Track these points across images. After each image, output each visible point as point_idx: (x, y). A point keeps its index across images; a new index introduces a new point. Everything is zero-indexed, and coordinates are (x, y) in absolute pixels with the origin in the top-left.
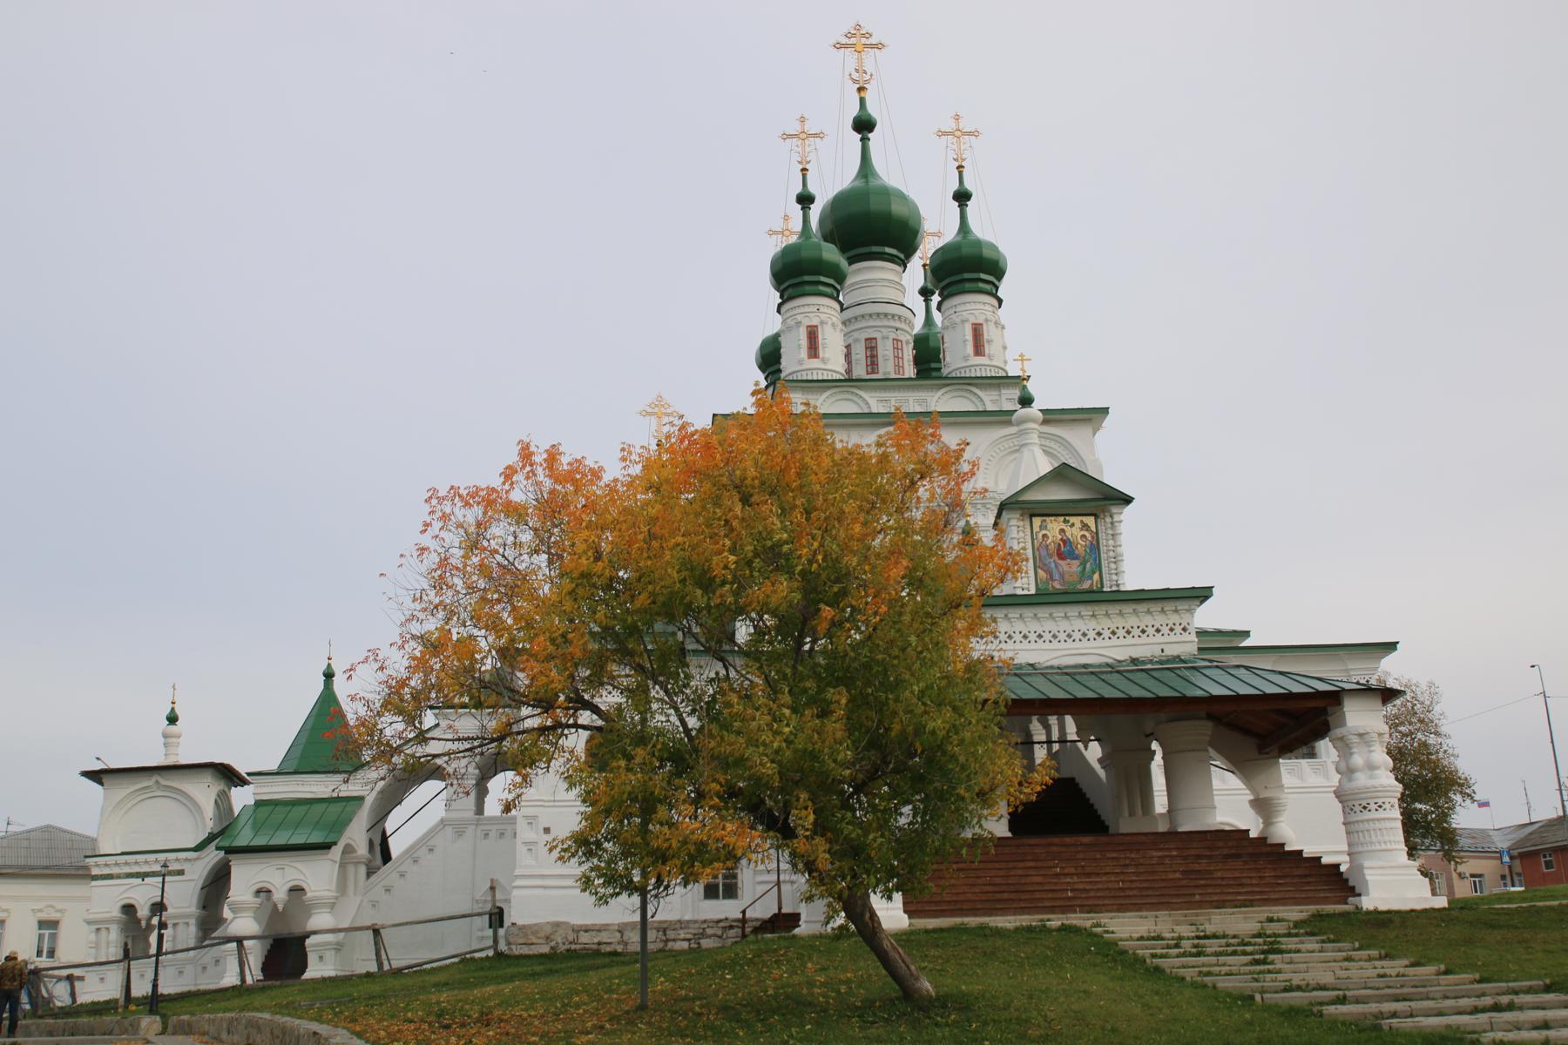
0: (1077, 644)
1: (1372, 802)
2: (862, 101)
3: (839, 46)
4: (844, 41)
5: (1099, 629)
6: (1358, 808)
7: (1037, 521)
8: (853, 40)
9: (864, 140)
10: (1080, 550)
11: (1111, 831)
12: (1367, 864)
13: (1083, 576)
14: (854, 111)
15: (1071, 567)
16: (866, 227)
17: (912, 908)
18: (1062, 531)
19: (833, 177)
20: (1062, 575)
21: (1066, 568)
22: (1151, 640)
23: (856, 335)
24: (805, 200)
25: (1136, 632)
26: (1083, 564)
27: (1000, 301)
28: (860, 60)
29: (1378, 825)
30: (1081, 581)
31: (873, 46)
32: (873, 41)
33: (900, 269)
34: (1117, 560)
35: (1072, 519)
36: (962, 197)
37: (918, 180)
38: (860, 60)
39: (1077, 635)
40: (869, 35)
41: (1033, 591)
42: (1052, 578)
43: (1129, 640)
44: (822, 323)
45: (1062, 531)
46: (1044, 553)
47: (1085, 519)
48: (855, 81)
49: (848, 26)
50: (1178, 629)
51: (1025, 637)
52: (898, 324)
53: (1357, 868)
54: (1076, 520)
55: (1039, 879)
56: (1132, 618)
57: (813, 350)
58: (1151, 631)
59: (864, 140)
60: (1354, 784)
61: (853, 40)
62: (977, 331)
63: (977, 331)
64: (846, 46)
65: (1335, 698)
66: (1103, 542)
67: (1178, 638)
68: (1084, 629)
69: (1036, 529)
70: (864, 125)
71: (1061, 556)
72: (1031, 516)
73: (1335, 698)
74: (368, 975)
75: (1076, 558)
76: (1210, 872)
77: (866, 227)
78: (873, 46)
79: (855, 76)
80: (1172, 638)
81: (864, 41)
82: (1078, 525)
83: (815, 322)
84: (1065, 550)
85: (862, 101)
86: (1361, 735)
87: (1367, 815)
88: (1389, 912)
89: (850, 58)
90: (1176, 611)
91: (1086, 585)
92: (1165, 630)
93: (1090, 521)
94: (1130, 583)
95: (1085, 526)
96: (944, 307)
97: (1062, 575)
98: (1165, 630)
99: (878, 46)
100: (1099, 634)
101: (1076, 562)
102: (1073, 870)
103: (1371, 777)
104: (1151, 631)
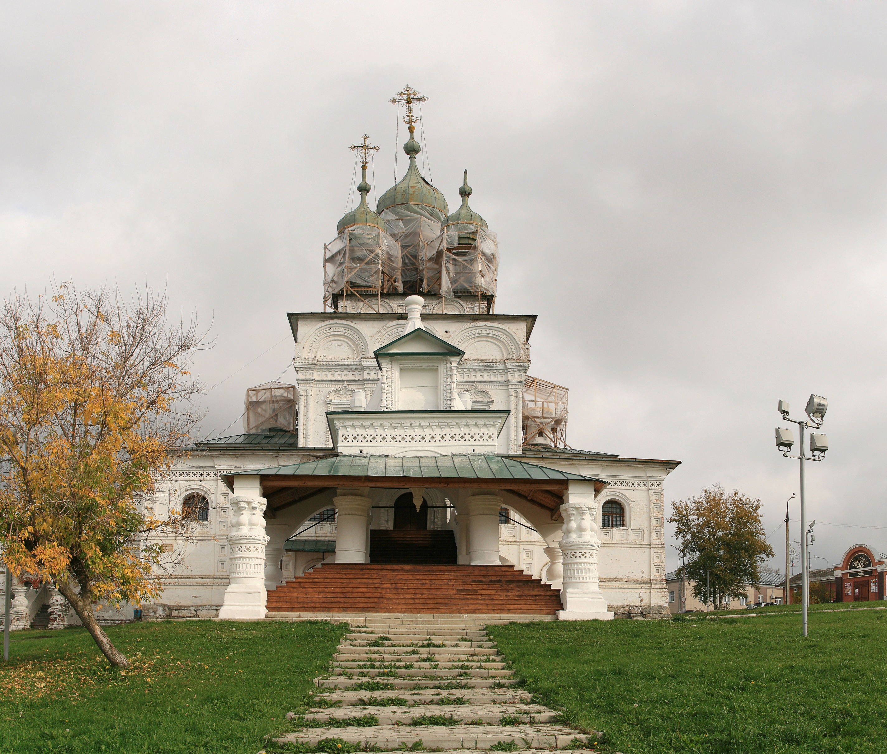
0: (418, 444)
1: (578, 552)
6: (578, 555)
11: (461, 560)
17: (273, 605)
19: (386, 176)
22: (467, 443)
24: (364, 189)
25: (457, 437)
39: (418, 438)
40: (415, 93)
43: (453, 442)
51: (627, 484)
53: (565, 592)
55: (365, 590)
58: (467, 437)
60: (568, 540)
65: (565, 483)
67: (485, 443)
73: (565, 483)
76: (476, 591)
78: (418, 100)
86: (577, 508)
87: (583, 560)
88: (576, 621)
92: (477, 437)
98: (477, 437)
99: (422, 99)
102: (389, 586)
103: (238, 531)
104: (467, 437)
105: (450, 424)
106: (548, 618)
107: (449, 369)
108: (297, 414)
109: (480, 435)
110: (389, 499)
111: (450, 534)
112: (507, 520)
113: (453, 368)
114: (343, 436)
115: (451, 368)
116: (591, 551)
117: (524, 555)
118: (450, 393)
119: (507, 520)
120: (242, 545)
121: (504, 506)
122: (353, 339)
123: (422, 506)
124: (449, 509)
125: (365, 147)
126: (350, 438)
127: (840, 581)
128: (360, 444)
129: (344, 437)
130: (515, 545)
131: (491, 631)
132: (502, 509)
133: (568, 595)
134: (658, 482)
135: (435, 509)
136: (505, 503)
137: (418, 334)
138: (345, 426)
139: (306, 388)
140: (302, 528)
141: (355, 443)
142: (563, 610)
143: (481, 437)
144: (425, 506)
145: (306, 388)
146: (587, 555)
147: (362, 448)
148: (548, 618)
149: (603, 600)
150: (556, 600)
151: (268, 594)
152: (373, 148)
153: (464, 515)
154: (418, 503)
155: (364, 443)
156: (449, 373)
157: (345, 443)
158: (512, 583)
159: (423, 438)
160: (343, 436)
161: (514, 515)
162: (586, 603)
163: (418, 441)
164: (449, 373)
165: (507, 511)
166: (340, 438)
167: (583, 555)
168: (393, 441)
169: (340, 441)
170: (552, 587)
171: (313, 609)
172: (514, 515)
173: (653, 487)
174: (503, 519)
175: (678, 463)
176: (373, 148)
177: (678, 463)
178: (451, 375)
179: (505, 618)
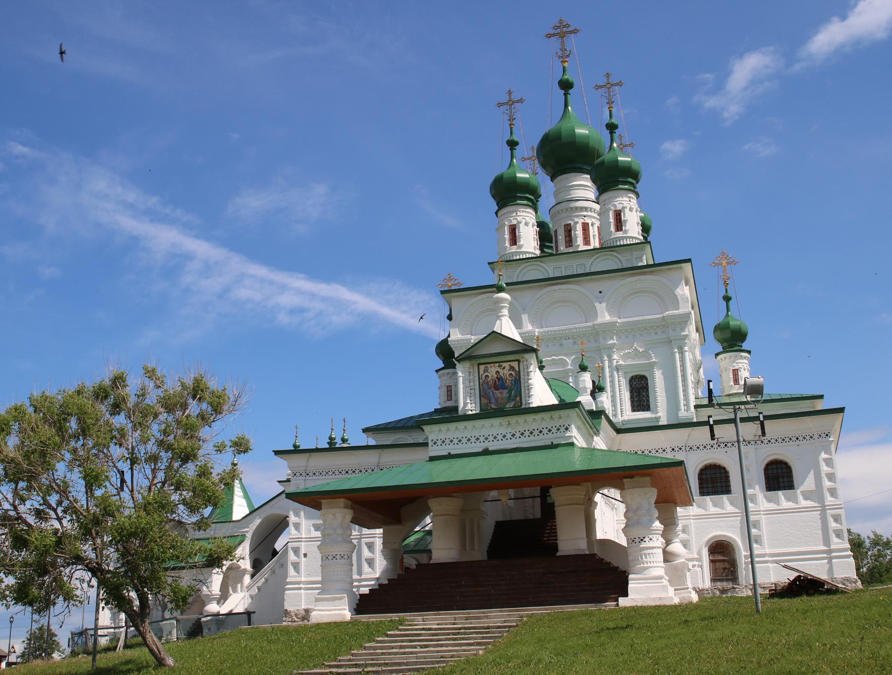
3: (549, 36)
4: (552, 32)
7: (482, 367)
13: (509, 399)
15: (502, 394)
18: (498, 372)
20: (497, 400)
21: (499, 395)
26: (510, 392)
28: (563, 43)
32: (570, 29)
34: (529, 388)
35: (504, 365)
38: (563, 43)
42: (490, 403)
44: (624, 208)
45: (498, 372)
46: (486, 387)
52: (585, 213)
57: (514, 240)
66: (522, 377)
69: (481, 372)
71: (496, 388)
72: (479, 365)
75: (506, 388)
81: (565, 29)
82: (508, 368)
89: (555, 42)
90: (560, 417)
93: (515, 364)
94: (534, 405)
95: (512, 368)
96: (500, 214)
97: (497, 400)
101: (506, 391)
143: (558, 429)
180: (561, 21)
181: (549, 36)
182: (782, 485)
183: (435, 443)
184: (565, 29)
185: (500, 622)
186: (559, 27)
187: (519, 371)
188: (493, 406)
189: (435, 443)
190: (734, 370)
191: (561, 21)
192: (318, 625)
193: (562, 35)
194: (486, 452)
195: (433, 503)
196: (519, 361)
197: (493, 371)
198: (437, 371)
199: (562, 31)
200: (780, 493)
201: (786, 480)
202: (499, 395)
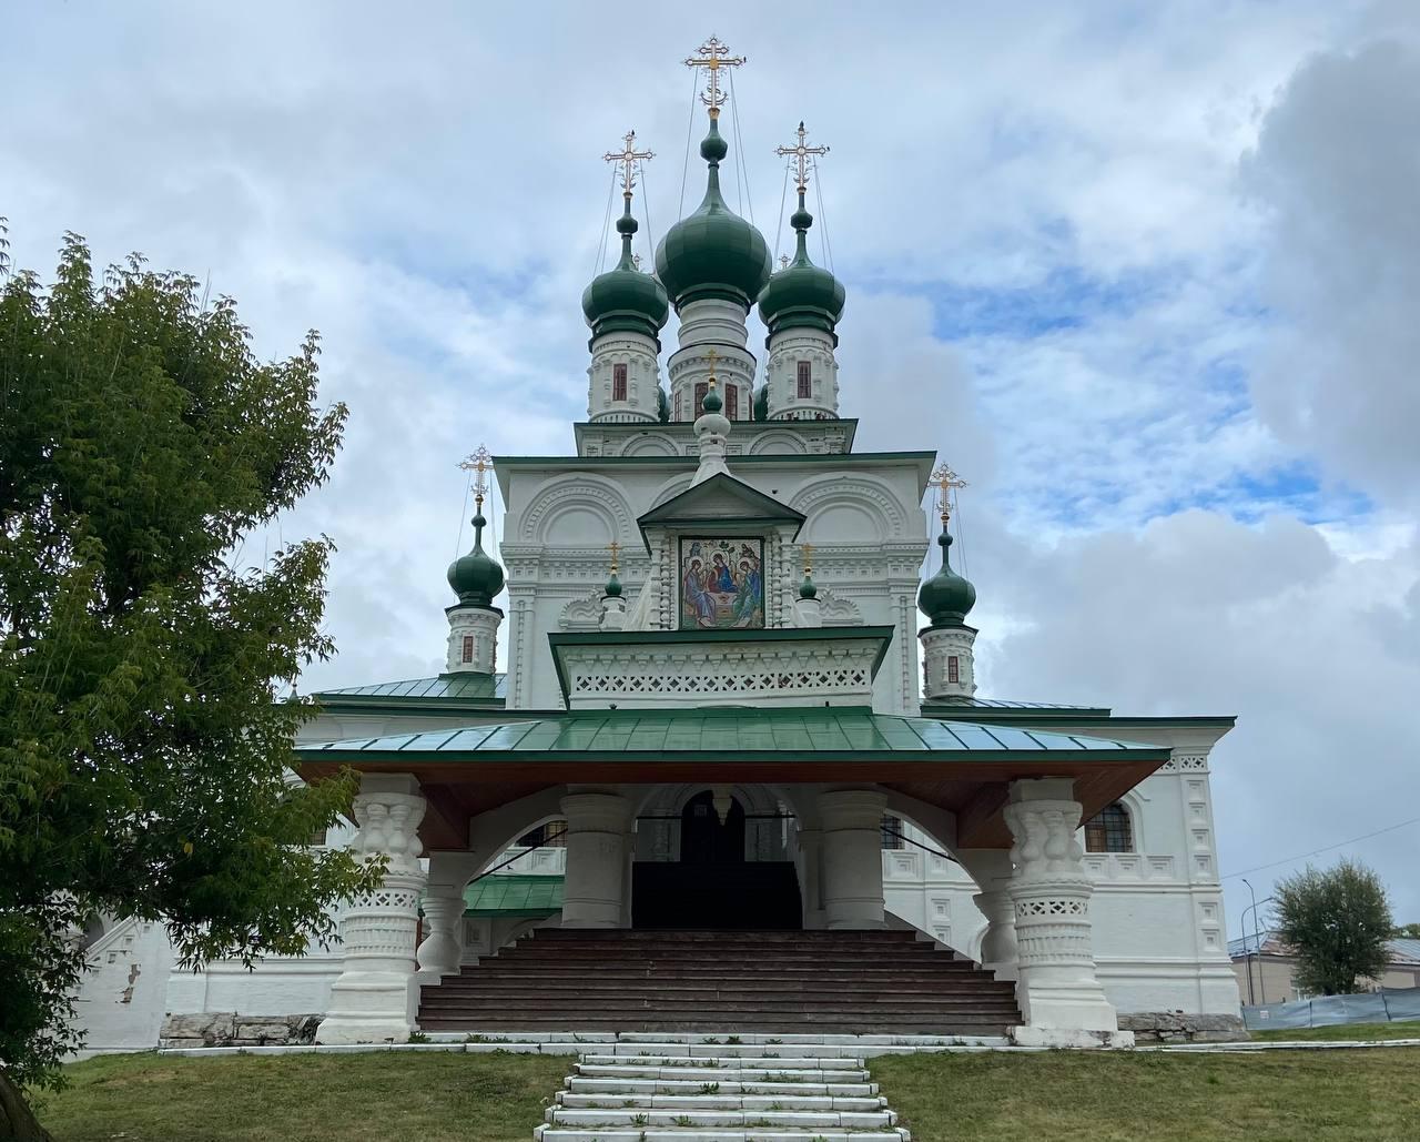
0: (721, 694)
2: (714, 124)
4: (698, 57)
5: (748, 675)
6: (1029, 909)
7: (688, 545)
8: (708, 56)
9: (714, 167)
10: (739, 581)
11: (810, 921)
12: (1033, 983)
14: (703, 134)
16: (714, 263)
19: (670, 202)
20: (713, 611)
22: (815, 690)
23: (686, 380)
24: (627, 227)
27: (835, 339)
28: (714, 80)
29: (1051, 932)
30: (737, 618)
31: (728, 62)
32: (730, 56)
33: (741, 309)
35: (732, 543)
36: (802, 222)
37: (763, 212)
38: (714, 80)
41: (675, 628)
42: (700, 615)
46: (693, 583)
47: (748, 543)
48: (706, 102)
49: (702, 40)
50: (850, 678)
53: (1025, 986)
54: (737, 545)
56: (788, 662)
59: (714, 167)
61: (708, 56)
62: (804, 372)
63: (804, 372)
64: (699, 62)
66: (767, 571)
68: (730, 675)
70: (714, 151)
72: (681, 538)
74: (1229, 1019)
77: (714, 263)
78: (728, 62)
79: (707, 95)
80: (842, 689)
81: (719, 56)
82: (739, 550)
83: (625, 360)
84: (722, 580)
85: (714, 124)
87: (1039, 918)
91: (743, 624)
93: (755, 546)
95: (748, 552)
97: (713, 611)
98: (833, 679)
100: (730, 682)
101: (732, 596)
103: (1049, 869)
105: (619, 657)
106: (995, 1042)
107: (776, 550)
108: (495, 644)
109: (838, 675)
110: (668, 799)
111: (788, 869)
112: (896, 840)
113: (784, 549)
114: (579, 678)
115: (780, 548)
116: (1076, 901)
117: (932, 907)
118: (780, 596)
119: (896, 840)
120: (1025, 901)
121: (891, 813)
122: (602, 503)
123: (730, 813)
124: (784, 820)
125: (802, 151)
126: (594, 683)
127: (262, 942)
128: (610, 694)
129: (581, 681)
130: (925, 888)
131: (875, 1068)
132: (885, 820)
133: (1031, 993)
134: (1197, 758)
135: (759, 820)
136: (891, 806)
137: (718, 484)
138: (584, 661)
139: (521, 598)
140: (500, 860)
141: (602, 693)
142: (1023, 1024)
143: (841, 678)
144: (736, 812)
145: (521, 598)
146: (1068, 907)
147: (615, 703)
148: (995, 1042)
149: (1106, 1003)
150: (1004, 1004)
151: (422, 994)
152: (815, 151)
153: (814, 831)
154: (722, 808)
155: (619, 693)
156: (777, 558)
157: (584, 693)
158: (907, 973)
159: (603, 683)
160: (579, 678)
161: (910, 830)
162: (1065, 1010)
163: (721, 689)
164: (777, 558)
165: (896, 821)
166: (574, 684)
167: (1058, 908)
168: (602, 689)
169: (573, 689)
170: (997, 977)
171: (1321, 1039)
172: (910, 830)
173: (1187, 769)
174: (889, 839)
175: (1229, 722)
176: (815, 151)
177: (1229, 722)
178: (780, 562)
179: (928, 1043)
180: (714, 41)
181: (691, 63)
182: (1110, 843)
183: (585, 684)
184: (719, 56)
185: (754, 1079)
186: (709, 51)
187: (762, 560)
188: (707, 623)
189: (585, 684)
190: (952, 659)
191: (714, 41)
192: (348, 1062)
193: (714, 65)
194: (768, 697)
195: (578, 810)
196: (763, 540)
197: (709, 552)
198: (447, 610)
199: (714, 58)
200: (1112, 855)
201: (1118, 835)
202: (719, 602)
